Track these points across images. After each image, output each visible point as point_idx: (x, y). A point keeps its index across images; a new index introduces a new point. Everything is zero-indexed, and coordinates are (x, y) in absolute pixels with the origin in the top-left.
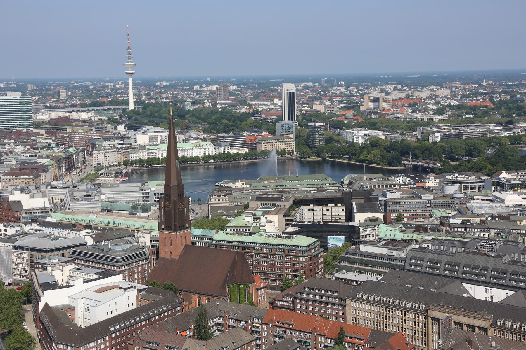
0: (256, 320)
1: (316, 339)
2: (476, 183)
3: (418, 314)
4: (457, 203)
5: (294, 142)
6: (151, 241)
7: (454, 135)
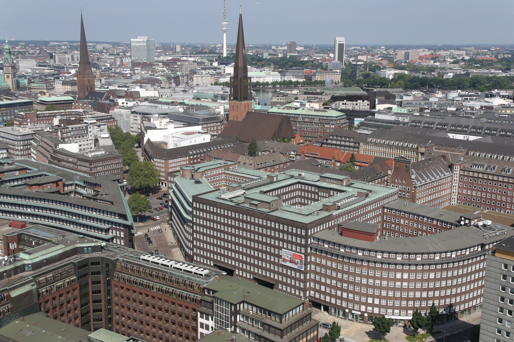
0: (292, 153)
1: (334, 164)
2: (474, 96)
3: (411, 151)
4: (456, 104)
5: (340, 76)
7: (463, 74)
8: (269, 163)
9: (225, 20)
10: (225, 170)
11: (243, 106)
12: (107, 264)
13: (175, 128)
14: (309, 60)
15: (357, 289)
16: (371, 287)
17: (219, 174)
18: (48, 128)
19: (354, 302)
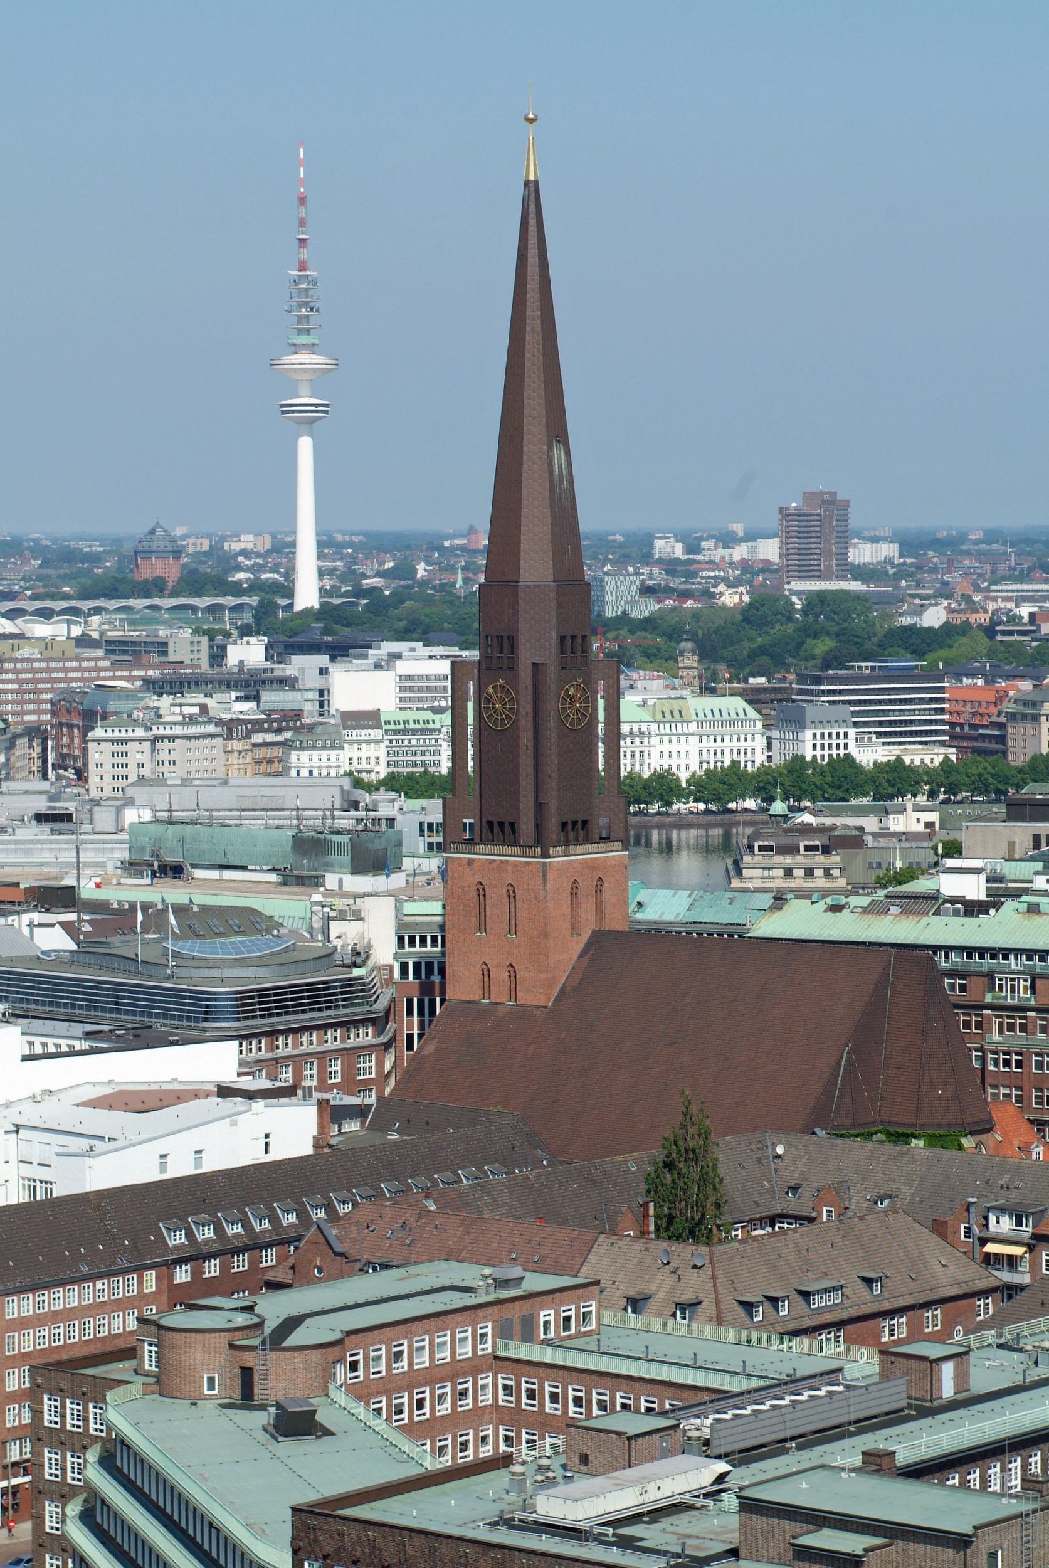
0: (1004, 1225)
6: (401, 939)
8: (835, 1299)
9: (304, 339)
10: (504, 1332)
11: (559, 885)
13: (25, 1058)
14: (958, 619)
17: (455, 1371)
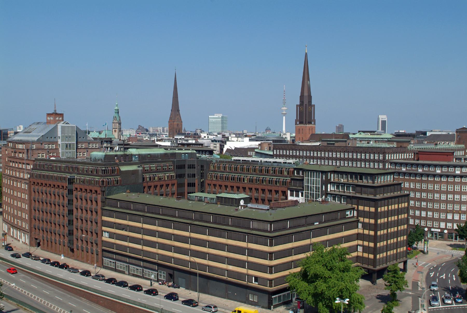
9: (284, 106)
12: (201, 165)
15: (436, 206)
16: (450, 202)
18: (147, 137)
19: (433, 219)
